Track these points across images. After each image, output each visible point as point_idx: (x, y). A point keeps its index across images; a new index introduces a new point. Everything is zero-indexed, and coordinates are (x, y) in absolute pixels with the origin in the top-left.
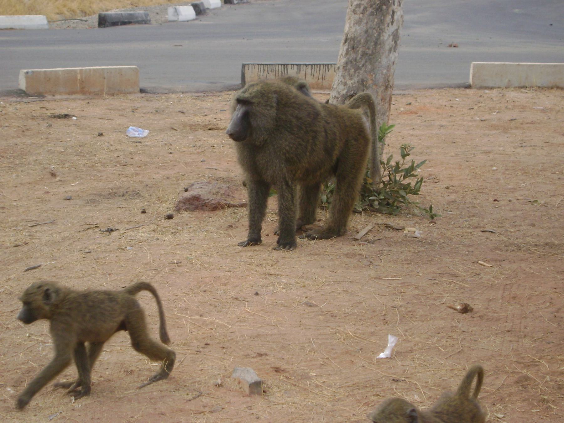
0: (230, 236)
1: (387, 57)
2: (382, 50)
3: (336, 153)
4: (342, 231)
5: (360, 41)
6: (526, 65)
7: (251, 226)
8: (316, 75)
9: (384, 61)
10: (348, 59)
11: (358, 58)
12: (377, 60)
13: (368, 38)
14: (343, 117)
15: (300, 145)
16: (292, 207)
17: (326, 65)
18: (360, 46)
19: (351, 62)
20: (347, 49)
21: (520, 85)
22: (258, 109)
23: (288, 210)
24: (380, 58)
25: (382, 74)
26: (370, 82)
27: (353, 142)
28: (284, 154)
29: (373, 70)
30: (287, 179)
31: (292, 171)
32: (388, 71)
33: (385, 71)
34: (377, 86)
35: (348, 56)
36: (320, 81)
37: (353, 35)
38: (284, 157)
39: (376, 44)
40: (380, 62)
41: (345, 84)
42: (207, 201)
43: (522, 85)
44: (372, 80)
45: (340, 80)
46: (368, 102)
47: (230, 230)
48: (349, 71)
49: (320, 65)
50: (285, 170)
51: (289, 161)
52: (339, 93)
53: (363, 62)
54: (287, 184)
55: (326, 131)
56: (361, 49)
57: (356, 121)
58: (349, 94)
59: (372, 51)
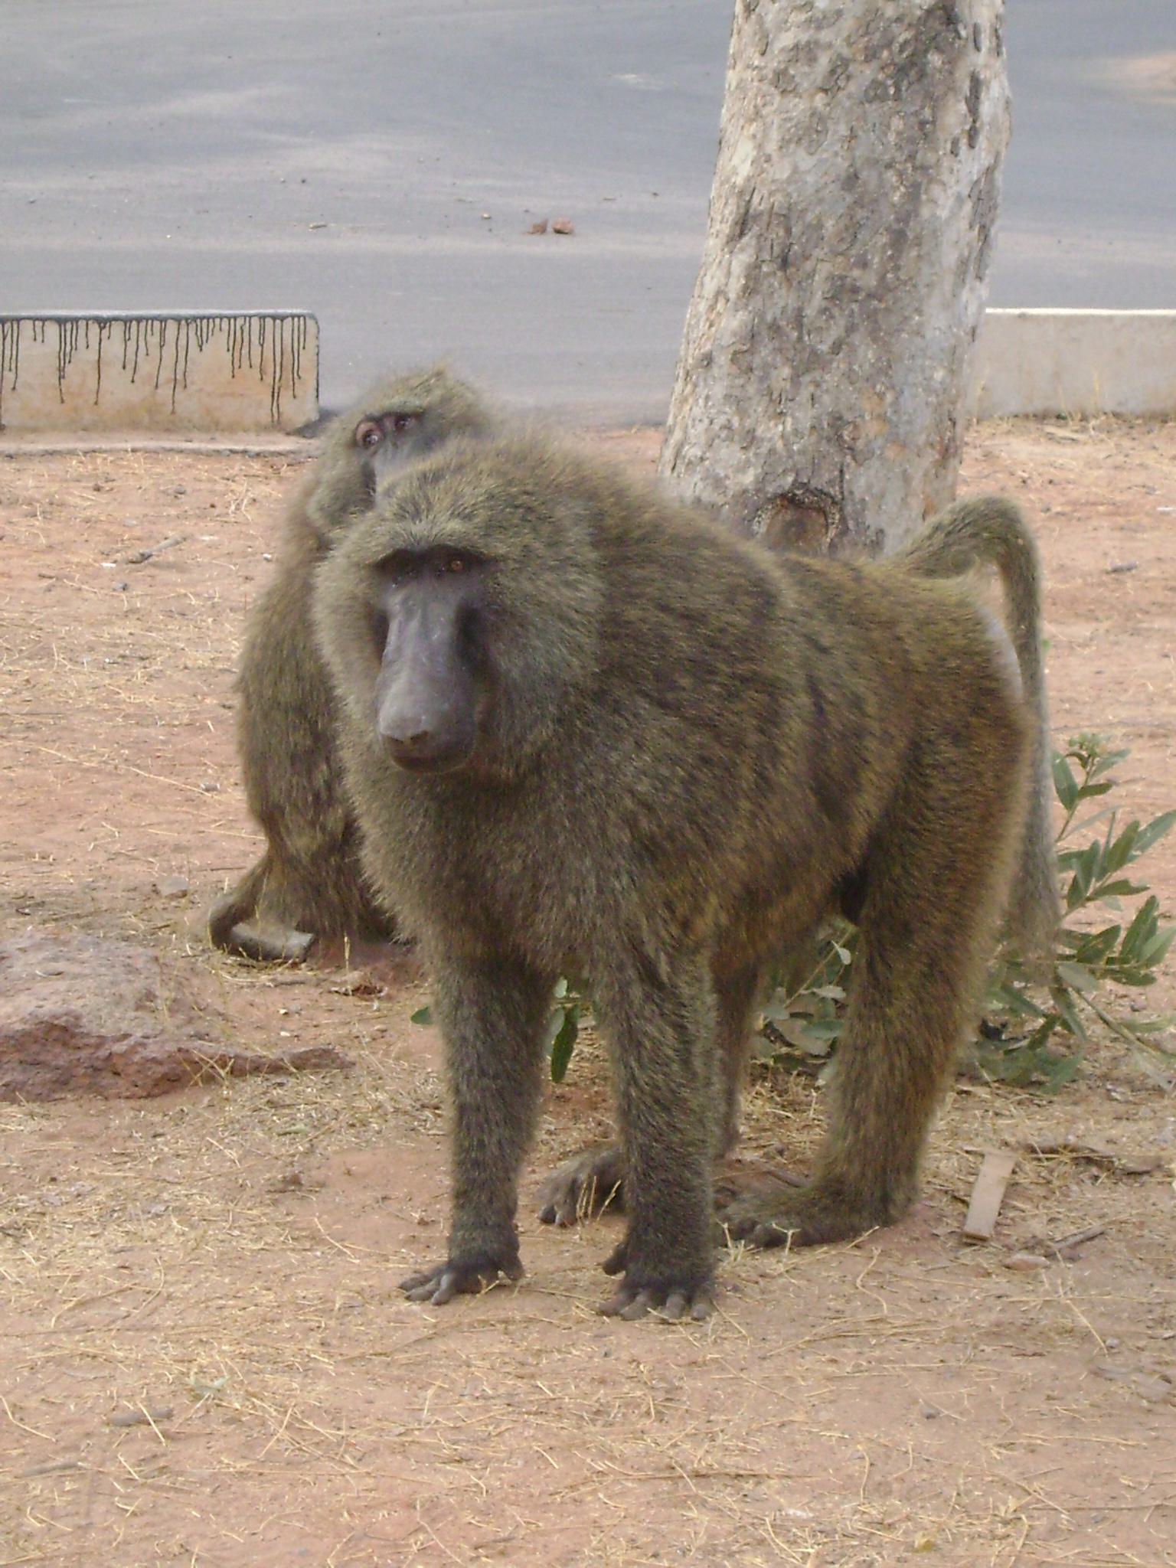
0: (315, 1239)
1: (947, 306)
2: (926, 269)
3: (867, 805)
4: (899, 1197)
5: (820, 226)
6: (1055, 317)
7: (462, 1196)
8: (146, 367)
9: (936, 323)
10: (761, 315)
11: (810, 312)
12: (906, 319)
13: (861, 214)
14: (890, 624)
15: (705, 761)
16: (685, 1093)
17: (190, 320)
18: (818, 253)
19: (775, 329)
20: (757, 266)
21: (1030, 409)
22: (528, 587)
23: (666, 1109)
24: (919, 311)
25: (929, 390)
26: (871, 428)
27: (947, 751)
28: (631, 822)
29: (884, 369)
30: (650, 950)
31: (669, 906)
32: (952, 372)
33: (939, 375)
34: (904, 446)
35: (757, 302)
36: (165, 391)
37: (778, 199)
38: (626, 837)
39: (898, 239)
40: (918, 333)
41: (750, 439)
42: (120, 1047)
43: (1038, 405)
44: (882, 418)
45: (721, 420)
46: (1005, 541)
47: (290, 1202)
48: (765, 377)
49: (163, 320)
50: (631, 905)
51: (649, 851)
52: (718, 483)
53: (836, 331)
54: (649, 974)
55: (814, 689)
56: (824, 269)
57: (960, 642)
58: (771, 489)
59: (882, 278)
